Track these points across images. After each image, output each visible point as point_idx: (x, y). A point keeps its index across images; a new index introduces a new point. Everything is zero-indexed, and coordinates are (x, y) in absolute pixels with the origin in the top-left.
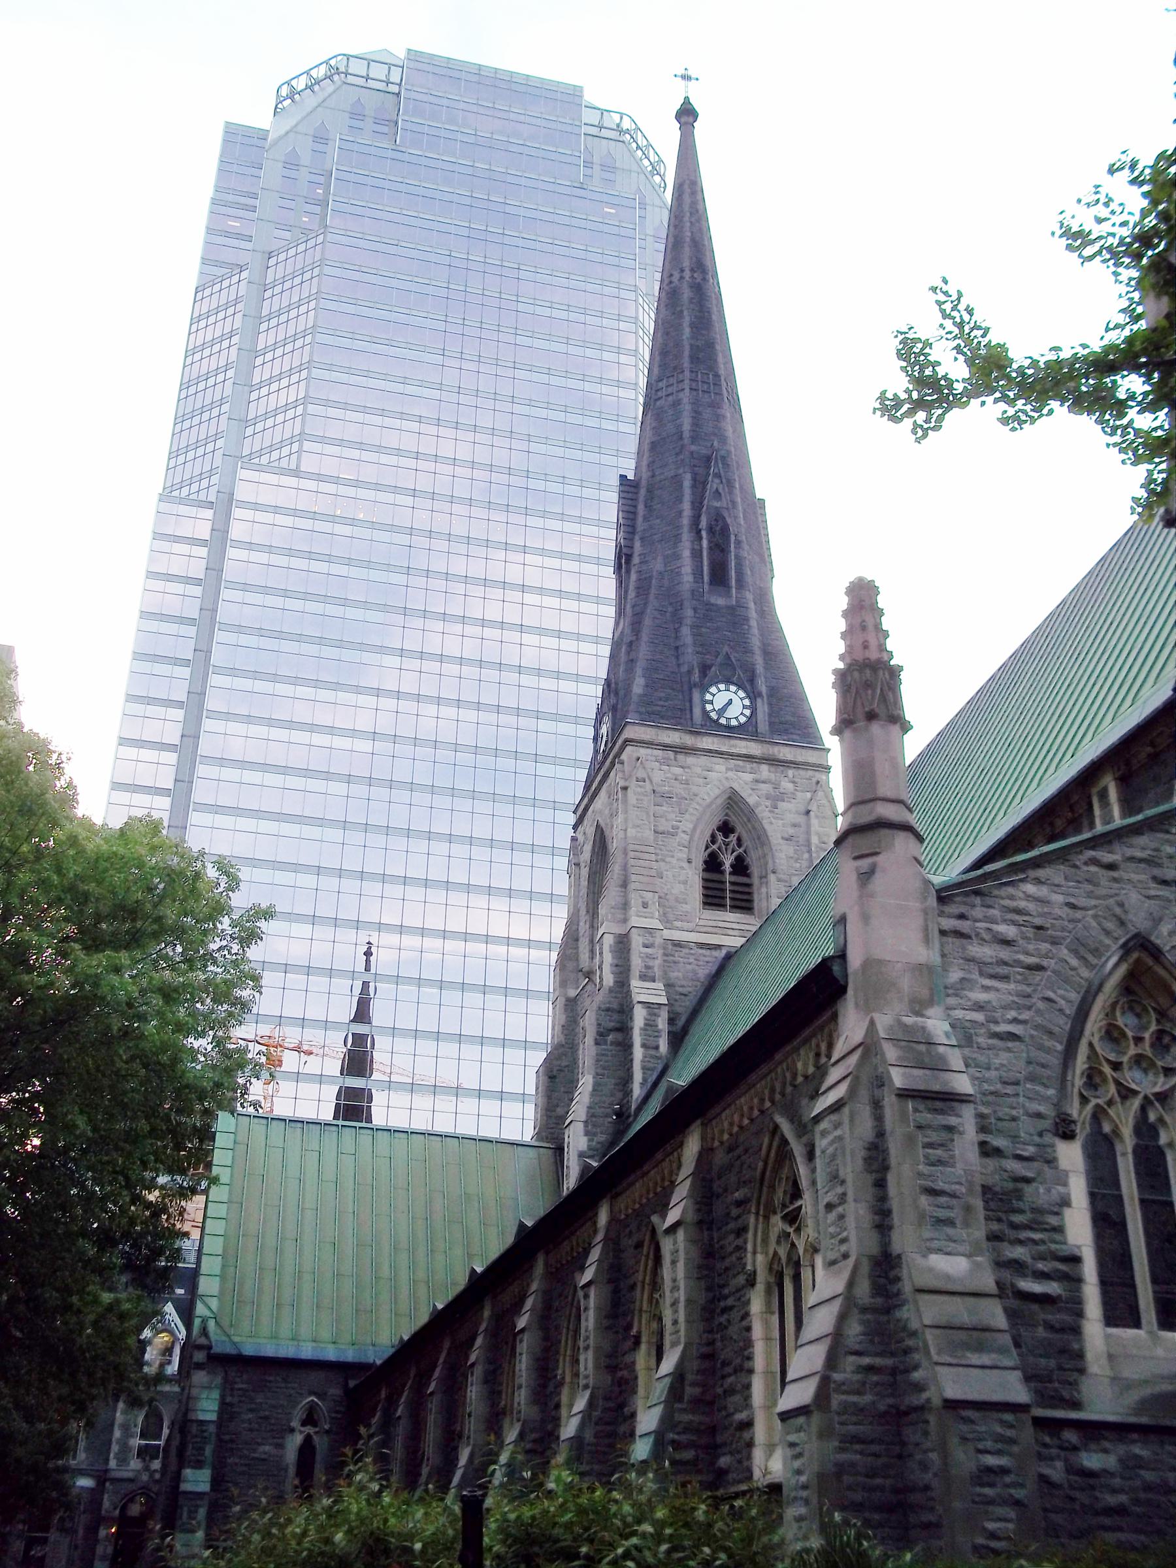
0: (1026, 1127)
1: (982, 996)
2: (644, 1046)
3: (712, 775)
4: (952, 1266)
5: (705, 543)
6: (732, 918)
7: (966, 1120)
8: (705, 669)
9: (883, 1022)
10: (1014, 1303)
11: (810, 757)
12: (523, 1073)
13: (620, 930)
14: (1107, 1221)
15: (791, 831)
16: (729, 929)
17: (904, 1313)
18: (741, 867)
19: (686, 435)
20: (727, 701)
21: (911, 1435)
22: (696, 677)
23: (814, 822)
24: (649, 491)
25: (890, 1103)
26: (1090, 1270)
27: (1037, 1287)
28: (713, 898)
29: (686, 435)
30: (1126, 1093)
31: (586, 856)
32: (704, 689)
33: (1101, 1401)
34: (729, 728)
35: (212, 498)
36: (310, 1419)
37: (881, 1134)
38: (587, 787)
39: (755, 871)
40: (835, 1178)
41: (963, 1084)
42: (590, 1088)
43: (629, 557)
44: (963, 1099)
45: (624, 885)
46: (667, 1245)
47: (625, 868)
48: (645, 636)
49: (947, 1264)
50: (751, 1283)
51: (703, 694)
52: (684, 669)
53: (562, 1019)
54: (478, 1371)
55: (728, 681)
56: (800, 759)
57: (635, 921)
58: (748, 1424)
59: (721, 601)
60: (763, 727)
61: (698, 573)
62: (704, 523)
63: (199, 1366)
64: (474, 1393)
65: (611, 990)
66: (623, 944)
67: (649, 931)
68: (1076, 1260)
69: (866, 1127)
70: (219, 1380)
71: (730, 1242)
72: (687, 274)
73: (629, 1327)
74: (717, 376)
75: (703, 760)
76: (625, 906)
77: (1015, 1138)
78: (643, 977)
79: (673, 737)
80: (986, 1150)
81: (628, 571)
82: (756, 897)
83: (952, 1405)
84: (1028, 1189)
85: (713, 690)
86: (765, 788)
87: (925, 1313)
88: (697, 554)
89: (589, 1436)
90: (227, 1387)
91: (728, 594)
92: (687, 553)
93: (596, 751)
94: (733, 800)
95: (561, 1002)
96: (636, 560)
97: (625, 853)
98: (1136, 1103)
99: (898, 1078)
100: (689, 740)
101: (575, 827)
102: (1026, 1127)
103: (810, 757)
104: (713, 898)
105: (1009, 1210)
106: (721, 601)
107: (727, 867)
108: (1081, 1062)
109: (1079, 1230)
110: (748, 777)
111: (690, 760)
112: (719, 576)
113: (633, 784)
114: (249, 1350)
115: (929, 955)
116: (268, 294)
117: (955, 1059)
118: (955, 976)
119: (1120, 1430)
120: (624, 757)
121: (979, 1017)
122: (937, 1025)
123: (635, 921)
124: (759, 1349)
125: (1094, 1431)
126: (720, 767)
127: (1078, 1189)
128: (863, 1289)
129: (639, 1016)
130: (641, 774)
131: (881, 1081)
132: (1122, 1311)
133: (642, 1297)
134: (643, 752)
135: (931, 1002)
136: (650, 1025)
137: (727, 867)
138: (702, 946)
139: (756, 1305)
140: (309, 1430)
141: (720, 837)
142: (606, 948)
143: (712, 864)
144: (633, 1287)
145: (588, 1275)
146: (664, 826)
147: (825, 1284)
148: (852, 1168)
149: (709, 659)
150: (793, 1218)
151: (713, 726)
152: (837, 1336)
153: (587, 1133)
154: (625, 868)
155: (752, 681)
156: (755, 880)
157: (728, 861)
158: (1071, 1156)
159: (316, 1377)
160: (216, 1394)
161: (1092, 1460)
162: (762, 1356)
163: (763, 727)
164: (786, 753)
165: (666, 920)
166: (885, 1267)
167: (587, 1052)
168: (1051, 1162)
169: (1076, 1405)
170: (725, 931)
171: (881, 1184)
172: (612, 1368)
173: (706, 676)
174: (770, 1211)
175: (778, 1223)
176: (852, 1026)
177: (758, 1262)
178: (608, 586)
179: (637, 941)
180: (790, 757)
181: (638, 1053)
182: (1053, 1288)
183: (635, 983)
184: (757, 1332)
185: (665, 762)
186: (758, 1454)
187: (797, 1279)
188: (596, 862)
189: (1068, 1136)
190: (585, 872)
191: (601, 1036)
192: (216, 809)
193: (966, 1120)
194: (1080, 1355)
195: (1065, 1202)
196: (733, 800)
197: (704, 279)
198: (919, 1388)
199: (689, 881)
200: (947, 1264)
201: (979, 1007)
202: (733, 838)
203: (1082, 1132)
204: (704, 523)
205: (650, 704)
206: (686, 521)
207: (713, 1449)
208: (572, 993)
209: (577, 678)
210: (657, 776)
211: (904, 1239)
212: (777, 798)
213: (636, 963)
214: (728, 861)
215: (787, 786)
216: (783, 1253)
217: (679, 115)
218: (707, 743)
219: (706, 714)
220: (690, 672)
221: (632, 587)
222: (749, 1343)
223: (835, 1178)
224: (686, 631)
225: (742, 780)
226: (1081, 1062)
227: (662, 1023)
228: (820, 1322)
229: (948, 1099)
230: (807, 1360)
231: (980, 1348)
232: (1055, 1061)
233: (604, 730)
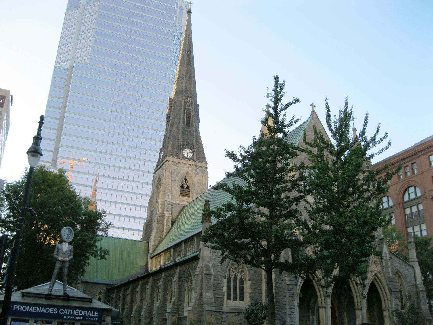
0: (220, 277)
1: (217, 260)
2: (166, 225)
3: (184, 168)
4: (209, 295)
5: (186, 116)
6: (185, 198)
7: (213, 276)
8: (184, 145)
9: (204, 264)
10: (216, 298)
11: (203, 165)
12: (141, 225)
13: (163, 200)
14: (229, 288)
15: (199, 181)
16: (185, 201)
17: (203, 300)
18: (188, 188)
19: (184, 91)
20: (187, 152)
21: (202, 313)
22: (182, 147)
23: (203, 179)
24: (175, 102)
25: (203, 275)
26: (226, 294)
27: (219, 296)
28: (182, 194)
29: (184, 91)
30: (233, 272)
31: (156, 181)
32: (183, 149)
33: (225, 309)
34: (188, 158)
35: (67, 67)
36: (100, 293)
37: (202, 278)
38: (157, 166)
39: (191, 188)
40: (196, 283)
41: (213, 273)
42: (155, 232)
43: (169, 117)
44: (213, 275)
45: (164, 191)
46: (173, 283)
47: (165, 187)
48: (172, 136)
49: (208, 295)
50: (185, 291)
51: (183, 151)
52: (179, 145)
53: (149, 215)
54: (139, 292)
55: (188, 148)
56: (202, 165)
57: (166, 199)
58: (183, 309)
59: (188, 130)
60: (195, 158)
61: (184, 123)
62: (186, 112)
63: (79, 283)
64: (138, 296)
65: (160, 213)
66: (163, 203)
67: (169, 201)
68: (224, 293)
69: (200, 278)
70: (83, 286)
71: (183, 285)
72: (187, 52)
73: (166, 292)
74: (191, 77)
75: (182, 165)
76: (164, 196)
77: (219, 278)
78: (167, 211)
79: (176, 160)
80: (215, 280)
81: (169, 120)
82: (190, 194)
83: (207, 311)
84: (220, 285)
85: (185, 150)
86: (194, 171)
87: (205, 300)
88: (184, 119)
89: (160, 307)
90: (85, 287)
91: (189, 128)
92: (182, 118)
93: (159, 159)
94: (187, 173)
95: (149, 211)
96: (171, 118)
97: (165, 184)
98: (234, 273)
99: (205, 272)
100: (179, 161)
101: (154, 174)
102: (220, 277)
103: (203, 165)
104: (182, 194)
105: (217, 287)
106: (188, 130)
107: (185, 188)
108: (228, 268)
109: (225, 289)
110: (191, 169)
111: (179, 165)
112: (188, 124)
113: (167, 170)
114: (88, 281)
115: (211, 255)
116: (84, 17)
117: (212, 270)
118: (214, 257)
119: (227, 312)
120: (166, 163)
121: (216, 263)
122: (210, 264)
123: (166, 199)
124: (186, 299)
125: (223, 312)
126: (185, 166)
127: (226, 285)
128: (199, 297)
129: (166, 219)
130: (169, 168)
131: (203, 272)
132: (229, 298)
133: (169, 288)
134: (170, 163)
135: (210, 261)
136: (168, 220)
137: (185, 188)
138: (179, 204)
139: (186, 294)
140: (100, 295)
141: (184, 181)
142: (160, 204)
143: (182, 187)
144: (167, 286)
145: (161, 283)
146: (173, 179)
147: (194, 296)
148: (198, 282)
149: (185, 143)
150: (191, 283)
151: (184, 157)
152: (195, 302)
153: (154, 241)
154: (165, 187)
155: (193, 148)
156: (191, 190)
157: (185, 186)
158: (225, 280)
159: (101, 286)
160: (83, 289)
161: (223, 316)
162: (186, 300)
163: (195, 158)
164: (199, 164)
165: (172, 198)
166: (201, 294)
167: (155, 225)
168: (223, 281)
169: (222, 310)
170: (183, 201)
171: (202, 284)
172: (164, 297)
173: (184, 146)
174: (188, 282)
175: (189, 284)
176: (200, 264)
177: (186, 288)
178: (165, 124)
179: (166, 203)
180: (199, 165)
181: (165, 226)
182: (221, 296)
183: (165, 212)
184: (185, 297)
185: (174, 165)
186: (184, 312)
187: (191, 291)
188: (158, 183)
189: (225, 278)
190: (156, 184)
191: (158, 222)
192: (66, 146)
193: (213, 276)
194: (223, 304)
195: (224, 286)
196: (187, 173)
197: (190, 53)
198: (203, 309)
199: (176, 190)
200: (208, 295)
201: (216, 262)
202: (187, 181)
203: (227, 278)
204: (186, 112)
205: (172, 152)
206: (182, 111)
207: (179, 311)
208: (152, 209)
209: (156, 140)
210: (172, 168)
211: (204, 292)
212: (196, 174)
213: (166, 208)
214: (185, 186)
215: (199, 171)
216: (190, 287)
217: (188, 12)
218: (183, 161)
219: (183, 155)
220: (180, 146)
221: (170, 124)
222: (184, 298)
223: (196, 283)
224: (180, 136)
225: (189, 170)
226: (228, 268)
227: (170, 221)
228: (193, 300)
229: (211, 275)
230: (191, 304)
231: (211, 304)
232: (225, 269)
233: (162, 155)
